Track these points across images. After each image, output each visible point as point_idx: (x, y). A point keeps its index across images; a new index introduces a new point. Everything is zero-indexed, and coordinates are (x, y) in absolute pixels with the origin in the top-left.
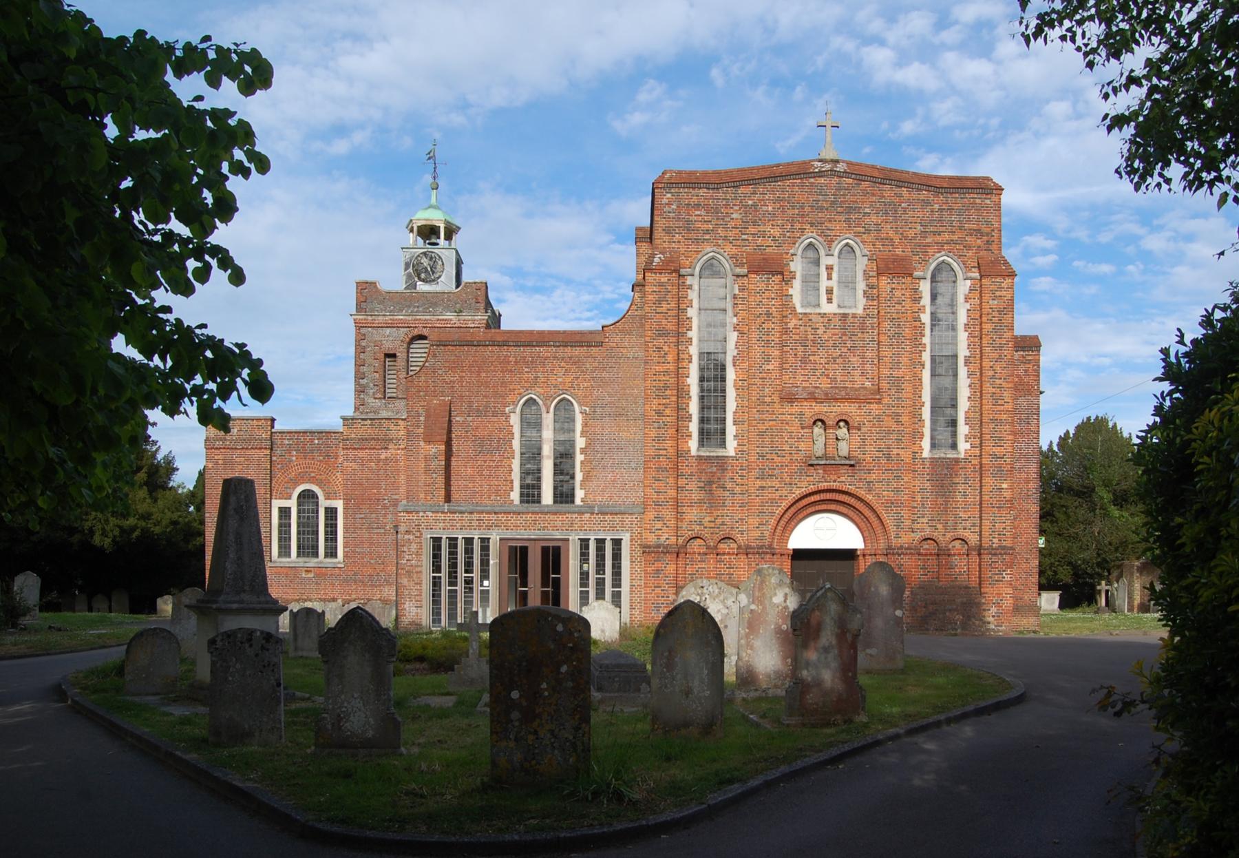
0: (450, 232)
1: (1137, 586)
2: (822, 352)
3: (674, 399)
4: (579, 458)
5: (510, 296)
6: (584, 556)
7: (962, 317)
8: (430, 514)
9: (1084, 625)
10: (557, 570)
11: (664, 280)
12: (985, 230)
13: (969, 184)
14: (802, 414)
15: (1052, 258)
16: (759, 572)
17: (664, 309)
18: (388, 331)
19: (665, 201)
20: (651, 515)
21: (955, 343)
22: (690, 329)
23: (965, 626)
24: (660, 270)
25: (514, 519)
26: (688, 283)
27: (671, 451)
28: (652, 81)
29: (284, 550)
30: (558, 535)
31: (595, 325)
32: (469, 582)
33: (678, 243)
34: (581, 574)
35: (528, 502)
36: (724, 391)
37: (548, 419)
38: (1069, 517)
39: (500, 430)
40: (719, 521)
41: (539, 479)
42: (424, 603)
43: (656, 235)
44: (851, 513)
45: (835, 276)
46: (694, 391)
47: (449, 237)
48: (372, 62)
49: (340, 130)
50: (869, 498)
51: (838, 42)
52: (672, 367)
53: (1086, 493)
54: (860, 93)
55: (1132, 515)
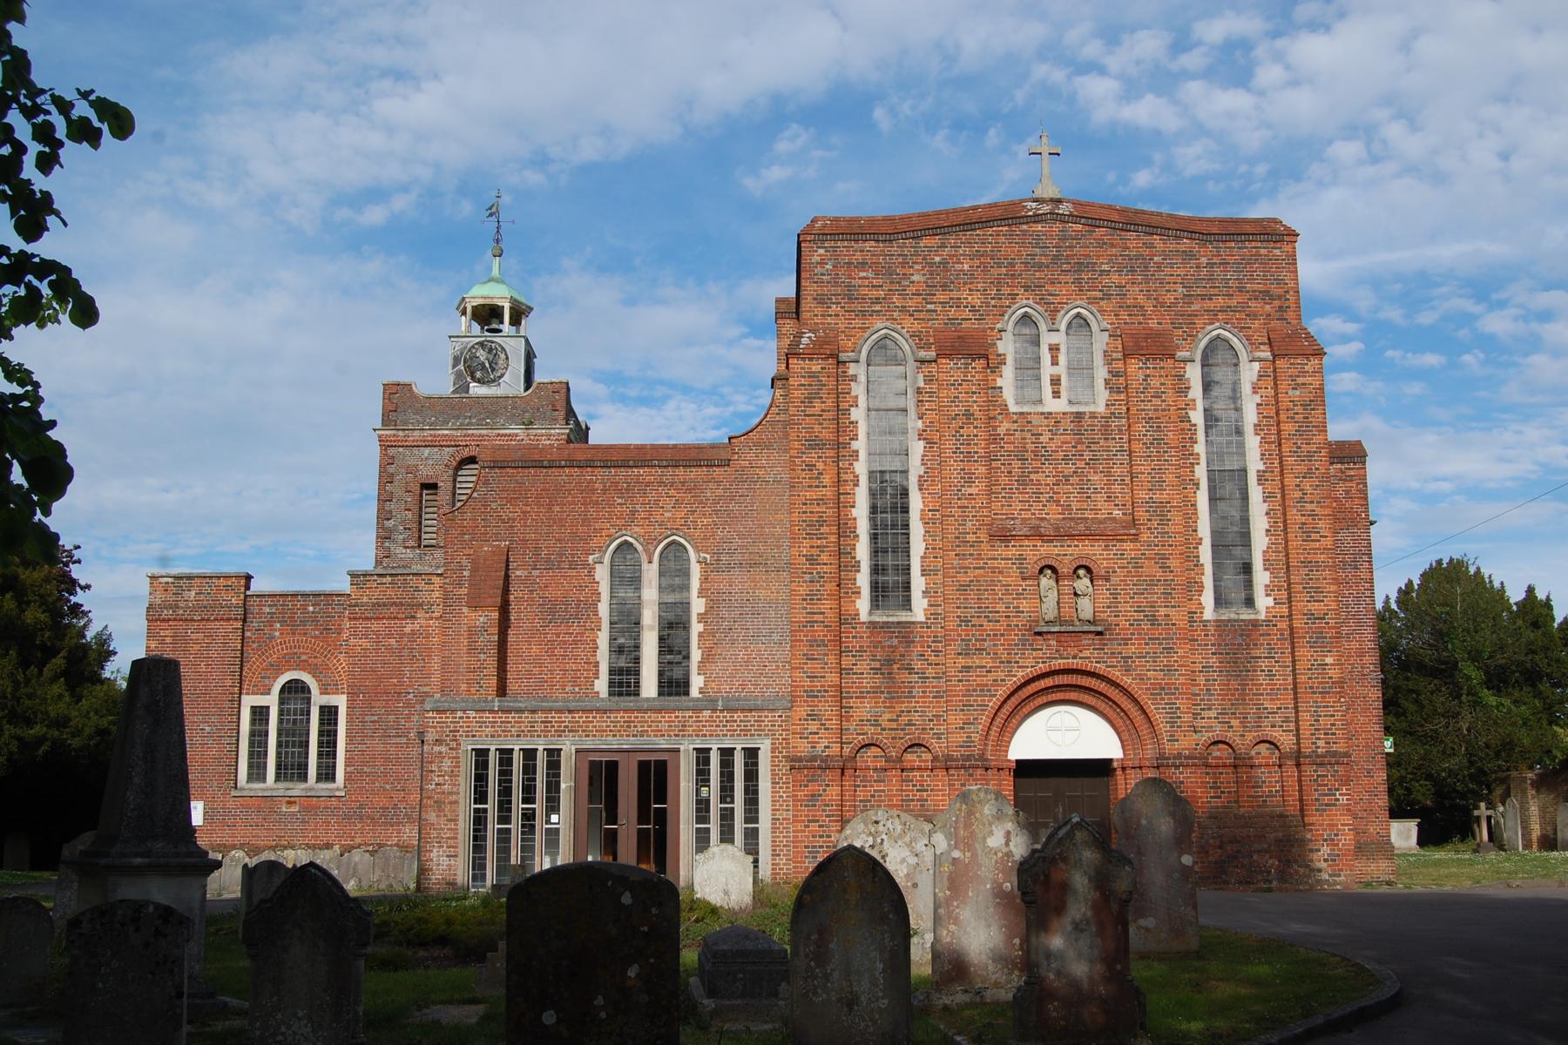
0: (518, 315)
1: (1534, 809)
2: (1048, 468)
3: (833, 538)
4: (696, 628)
5: (607, 409)
6: (702, 776)
7: (1250, 416)
8: (472, 714)
9: (1459, 872)
10: (662, 798)
11: (816, 368)
12: (1275, 290)
14: (1021, 558)
15: (1356, 347)
16: (964, 797)
17: (816, 410)
18: (427, 451)
19: (816, 259)
20: (802, 711)
22: (855, 438)
23: (1283, 876)
24: (810, 355)
25: (598, 720)
26: (851, 372)
27: (831, 616)
28: (795, 126)
29: (257, 771)
30: (663, 744)
31: (719, 436)
32: (529, 816)
33: (836, 318)
34: (699, 802)
35: (620, 694)
36: (906, 526)
37: (650, 572)
38: (1422, 707)
39: (581, 588)
40: (904, 719)
41: (637, 660)
42: (460, 850)
43: (804, 306)
44: (1102, 705)
45: (1062, 359)
47: (516, 321)
48: (420, 106)
49: (376, 194)
50: (1127, 681)
51: (1041, 71)
52: (829, 493)
53: (1445, 671)
54: (1073, 136)
55: (1515, 702)
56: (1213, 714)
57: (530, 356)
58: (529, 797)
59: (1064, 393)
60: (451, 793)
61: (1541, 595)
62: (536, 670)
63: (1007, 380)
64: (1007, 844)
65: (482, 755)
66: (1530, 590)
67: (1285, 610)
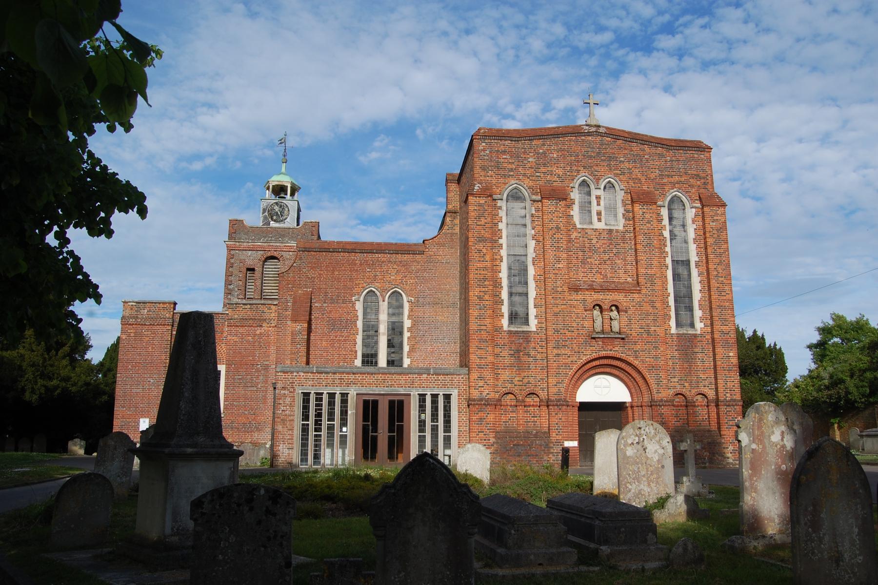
0: (294, 190)
2: (596, 256)
4: (406, 335)
6: (422, 408)
7: (691, 234)
10: (401, 419)
11: (482, 202)
13: (688, 144)
14: (584, 300)
17: (483, 223)
18: (250, 252)
21: (687, 252)
22: (501, 238)
23: (711, 461)
24: (479, 195)
26: (499, 205)
30: (402, 391)
32: (331, 428)
33: (491, 177)
37: (384, 306)
39: (348, 313)
40: (526, 380)
42: (295, 446)
45: (602, 203)
46: (505, 283)
47: (292, 194)
48: (220, 119)
49: (198, 157)
50: (636, 363)
52: (489, 264)
56: (676, 380)
57: (299, 210)
58: (331, 417)
59: (603, 220)
60: (290, 415)
61: (759, 334)
62: (325, 354)
63: (575, 212)
64: (782, 440)
65: (306, 395)
66: (755, 332)
67: (709, 329)
